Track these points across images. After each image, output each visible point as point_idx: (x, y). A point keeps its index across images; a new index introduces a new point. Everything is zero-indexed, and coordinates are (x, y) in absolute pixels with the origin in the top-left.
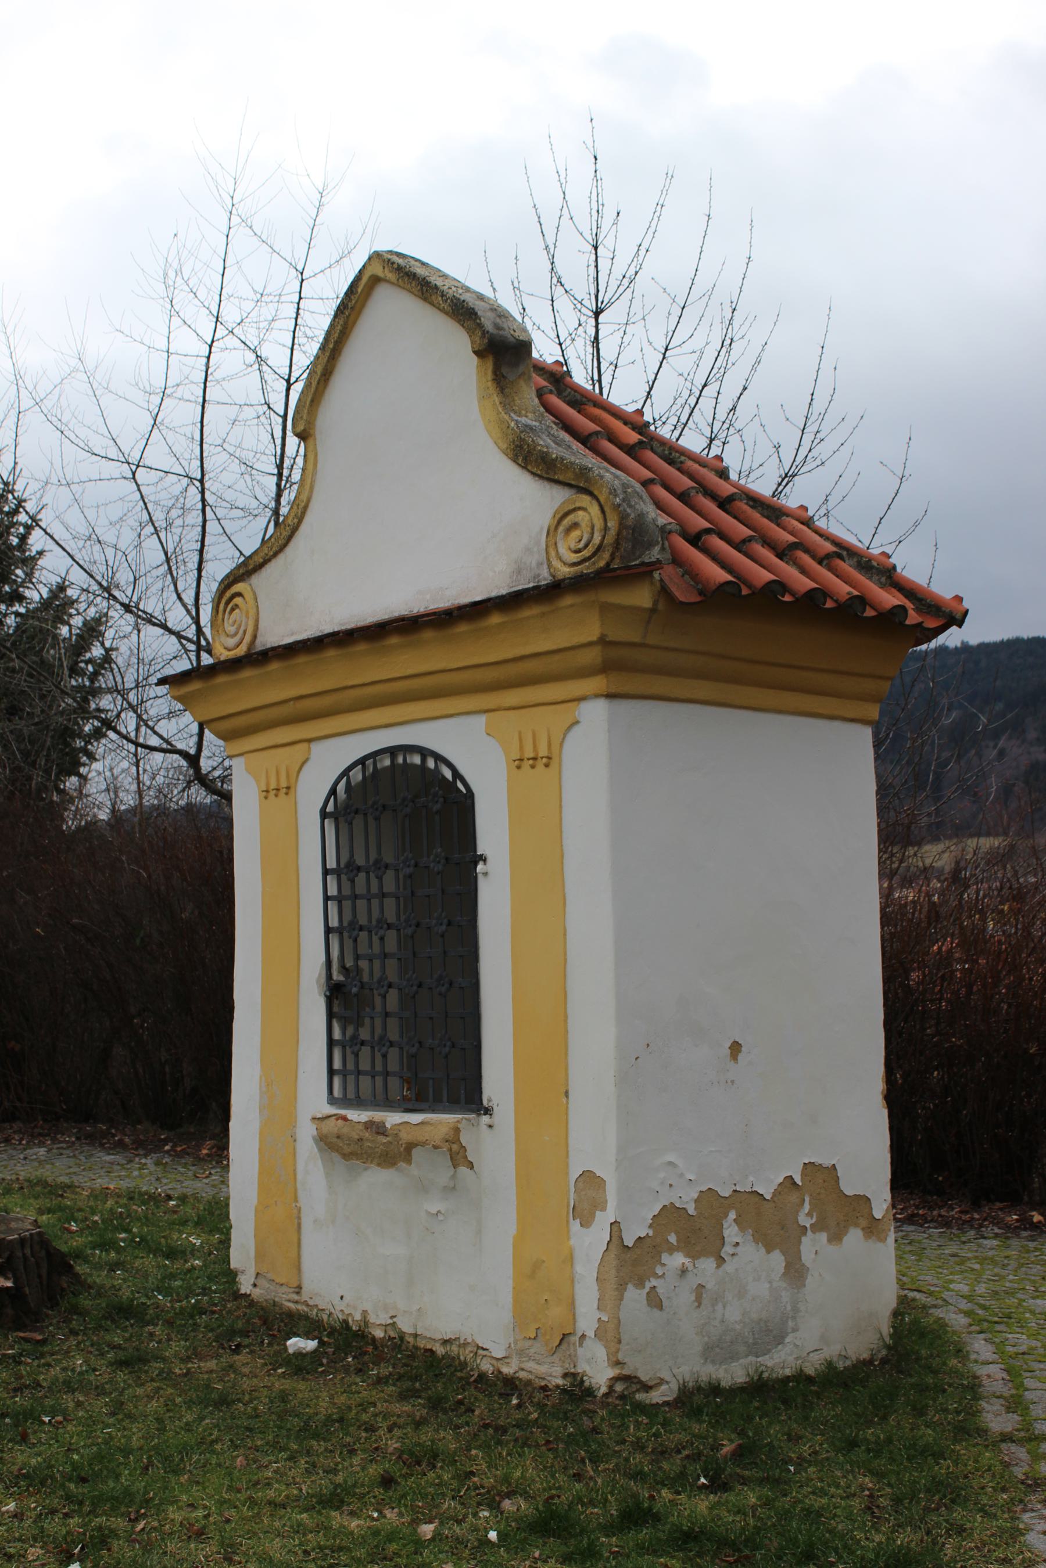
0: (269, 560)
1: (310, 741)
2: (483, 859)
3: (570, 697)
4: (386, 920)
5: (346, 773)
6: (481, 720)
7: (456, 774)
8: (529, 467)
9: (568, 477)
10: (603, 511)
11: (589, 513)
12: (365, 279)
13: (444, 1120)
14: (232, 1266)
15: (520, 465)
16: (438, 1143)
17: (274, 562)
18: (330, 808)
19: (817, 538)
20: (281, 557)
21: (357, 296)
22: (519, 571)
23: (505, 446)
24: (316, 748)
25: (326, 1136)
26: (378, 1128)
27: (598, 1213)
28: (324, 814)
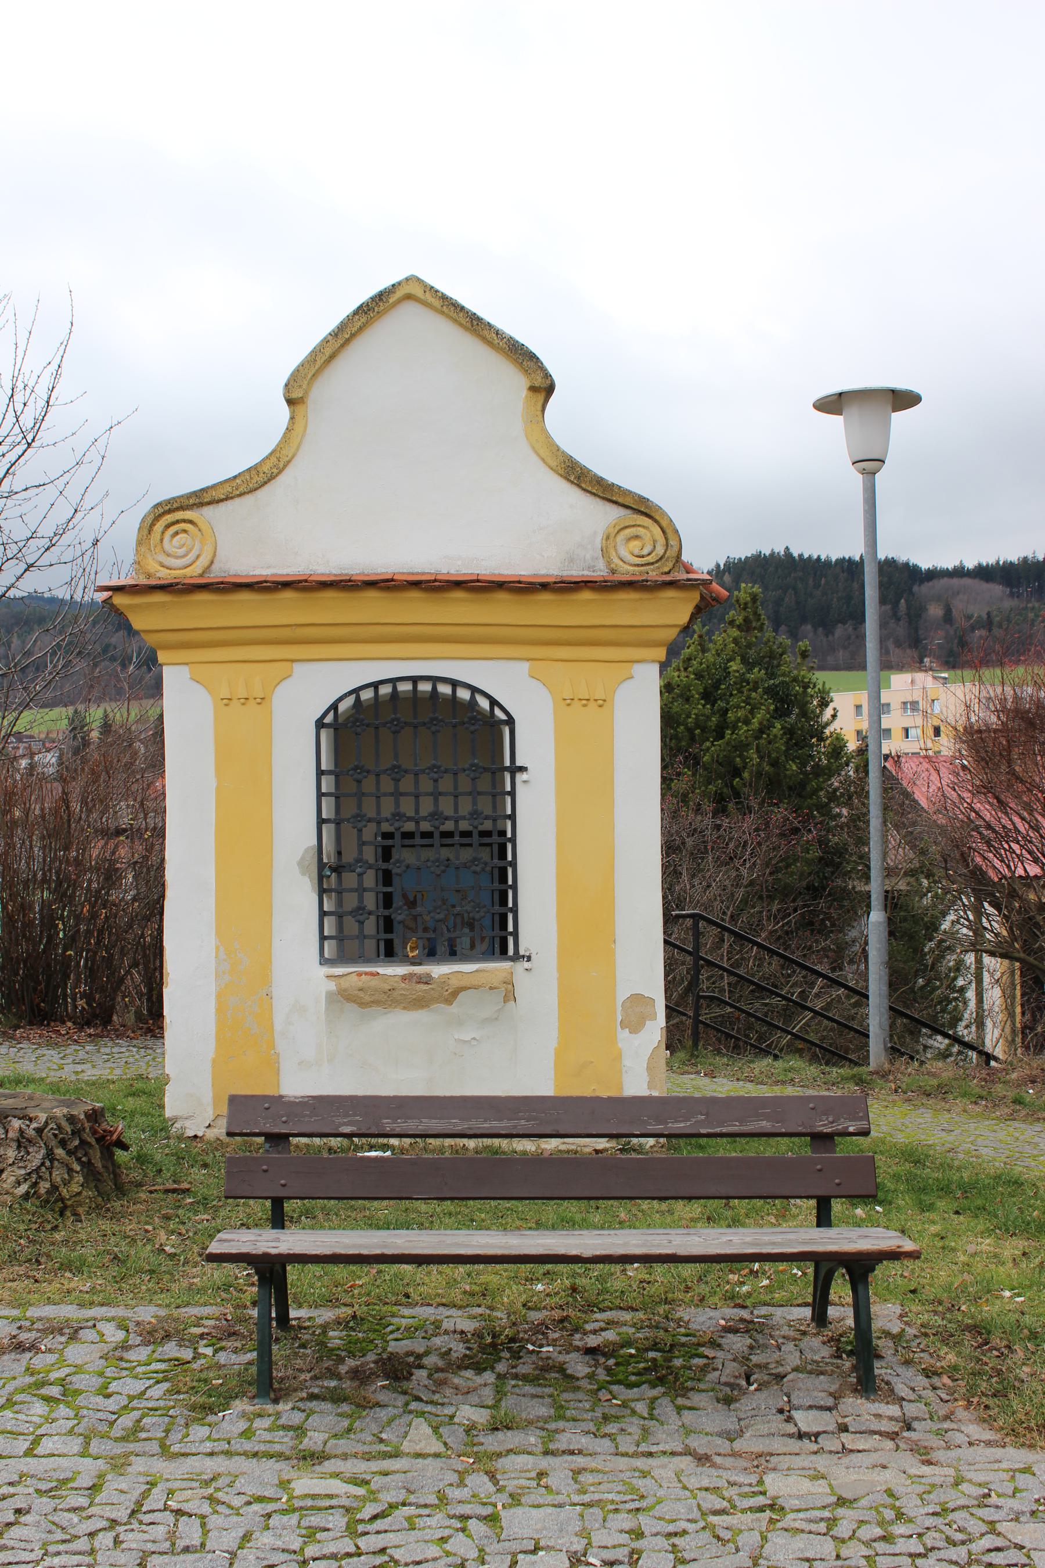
0: (232, 498)
1: (293, 661)
2: (516, 770)
3: (629, 659)
4: (442, 813)
5: (356, 691)
6: (525, 666)
7: (494, 702)
8: (583, 485)
9: (628, 501)
10: (664, 532)
11: (650, 531)
12: (399, 294)
13: (498, 967)
14: (168, 1113)
15: (572, 482)
16: (495, 984)
17: (237, 500)
18: (329, 719)
19: (178, 572)
20: (248, 499)
21: (387, 305)
22: (571, 560)
23: (554, 464)
24: (298, 668)
25: (345, 990)
26: (426, 980)
27: (648, 1022)
28: (320, 724)
